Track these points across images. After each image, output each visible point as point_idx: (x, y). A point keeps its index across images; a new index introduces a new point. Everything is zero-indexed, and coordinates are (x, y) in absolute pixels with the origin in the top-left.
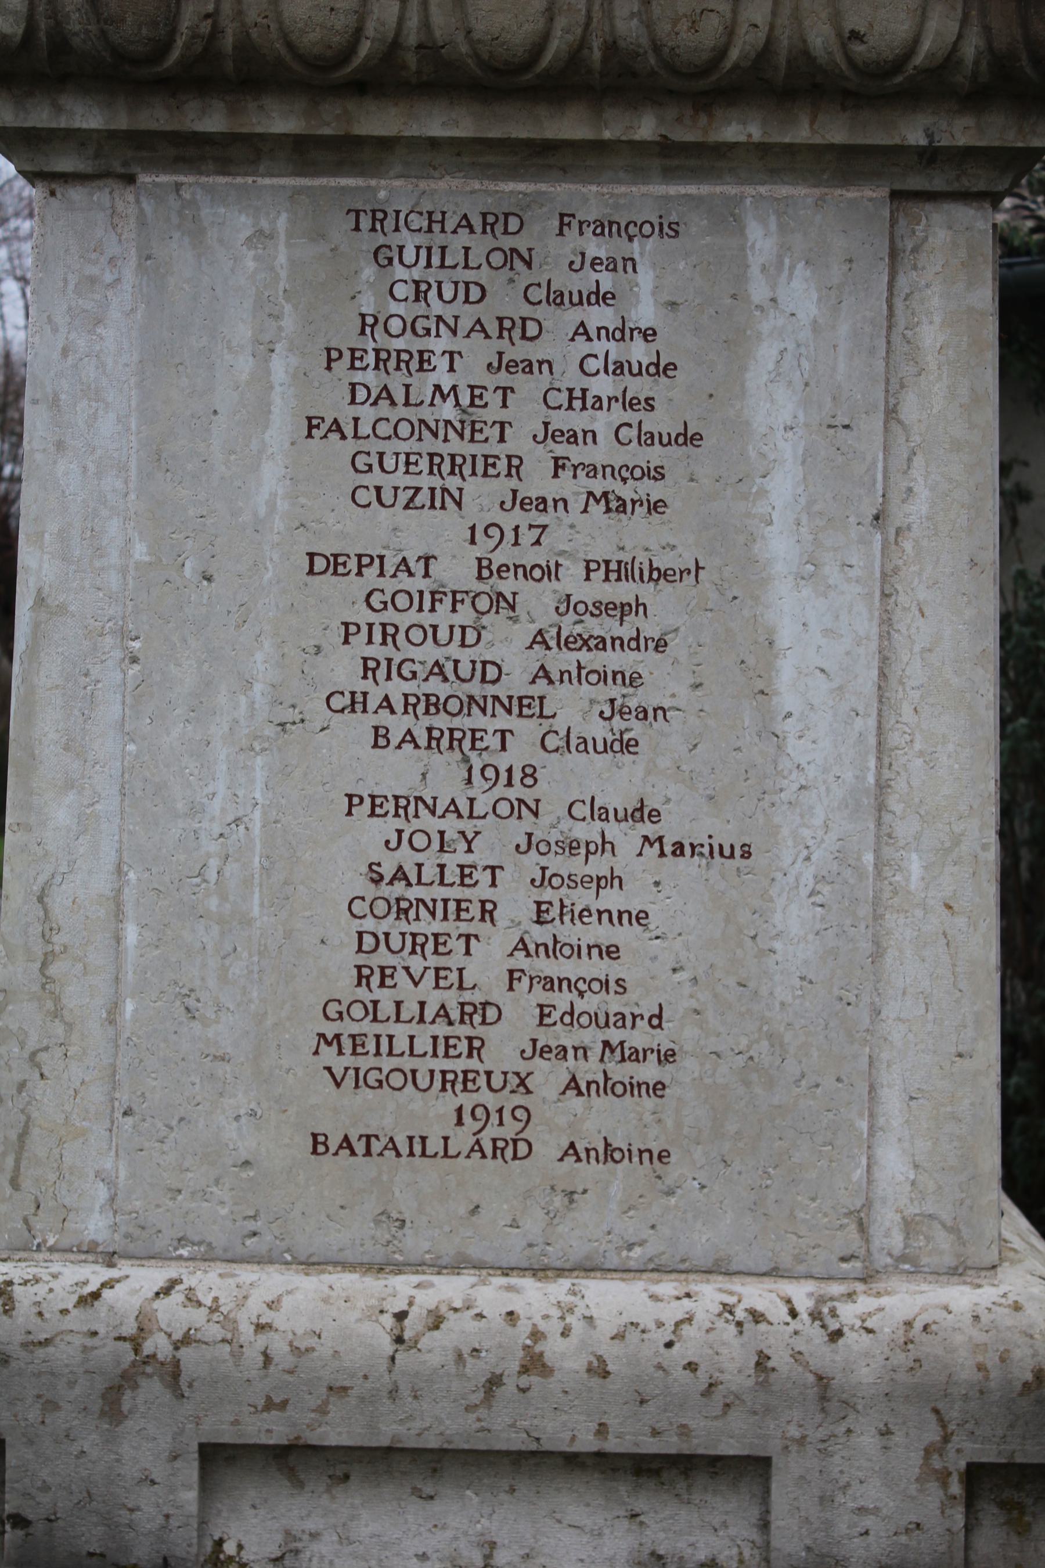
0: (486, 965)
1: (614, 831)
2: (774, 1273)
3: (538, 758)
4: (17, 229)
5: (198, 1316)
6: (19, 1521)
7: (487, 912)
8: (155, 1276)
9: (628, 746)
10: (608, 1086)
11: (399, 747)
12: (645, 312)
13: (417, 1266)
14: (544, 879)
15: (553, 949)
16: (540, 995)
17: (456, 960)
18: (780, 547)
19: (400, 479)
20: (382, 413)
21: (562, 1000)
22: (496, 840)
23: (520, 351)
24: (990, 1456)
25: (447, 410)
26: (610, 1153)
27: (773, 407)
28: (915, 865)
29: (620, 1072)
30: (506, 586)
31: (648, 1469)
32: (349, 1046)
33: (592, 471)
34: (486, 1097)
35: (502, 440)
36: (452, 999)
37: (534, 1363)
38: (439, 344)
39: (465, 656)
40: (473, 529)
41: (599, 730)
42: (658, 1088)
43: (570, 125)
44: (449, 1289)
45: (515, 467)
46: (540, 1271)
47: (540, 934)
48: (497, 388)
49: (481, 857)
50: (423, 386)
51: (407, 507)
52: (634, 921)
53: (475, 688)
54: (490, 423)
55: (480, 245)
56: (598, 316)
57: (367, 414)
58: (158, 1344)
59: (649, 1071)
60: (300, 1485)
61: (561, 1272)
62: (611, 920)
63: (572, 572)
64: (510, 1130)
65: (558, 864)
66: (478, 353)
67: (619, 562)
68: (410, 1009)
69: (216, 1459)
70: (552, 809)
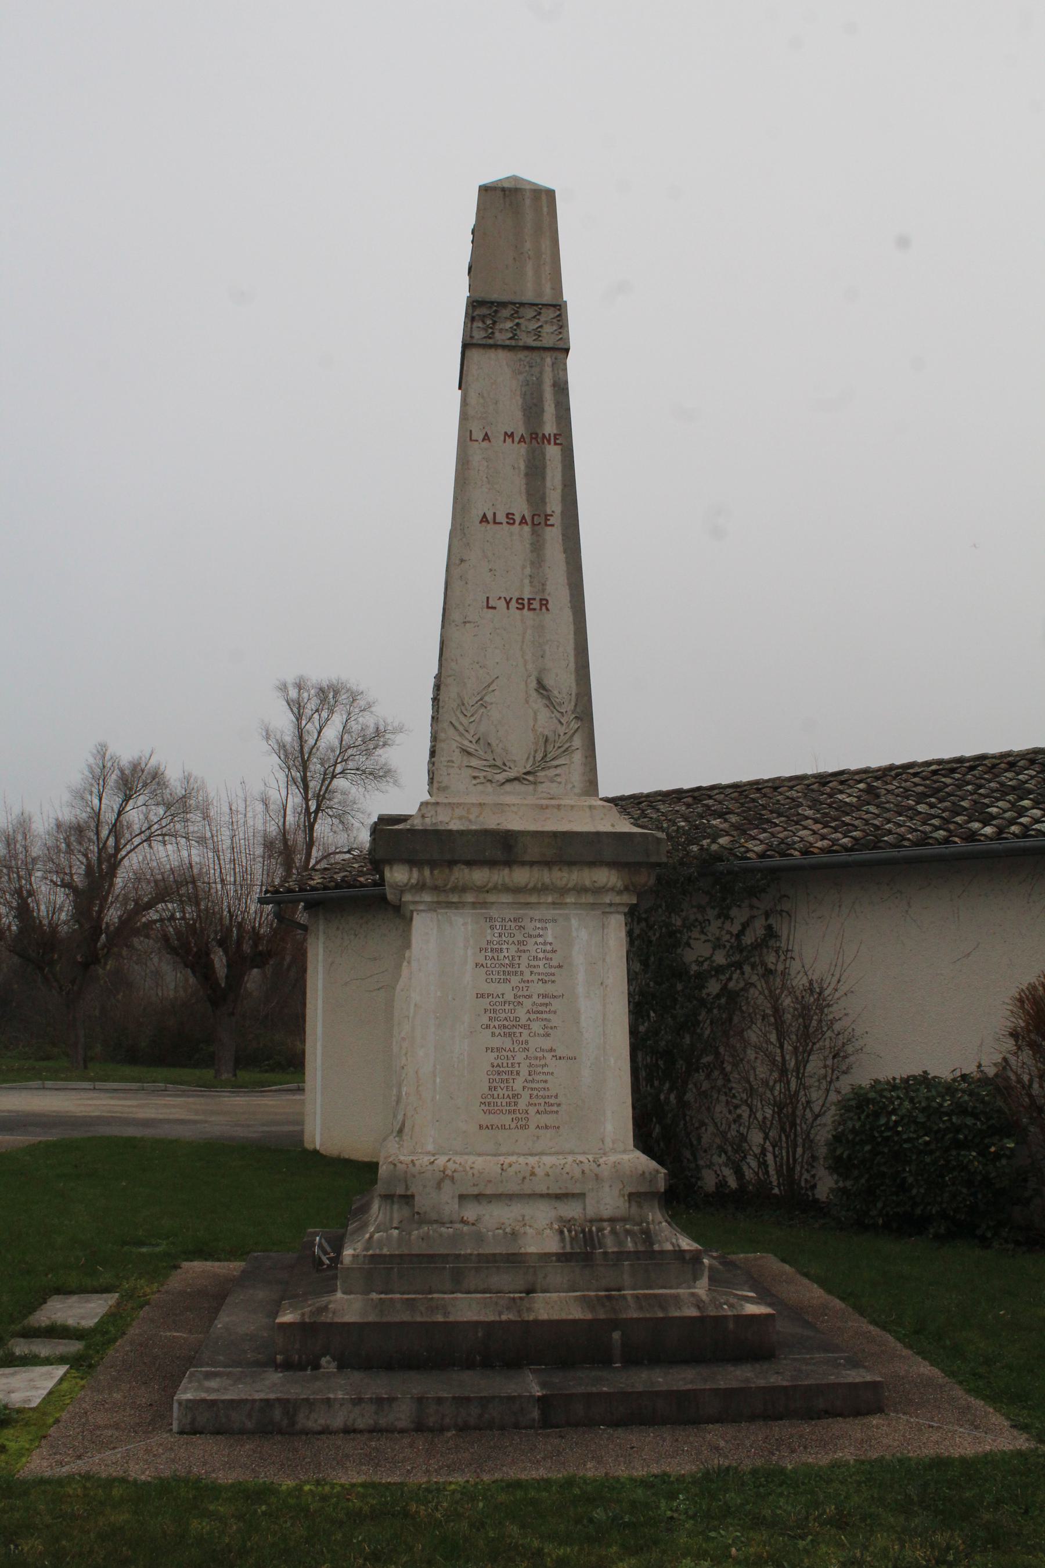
0: (518, 1085)
1: (546, 1054)
2: (584, 1153)
3: (529, 1038)
5: (457, 1166)
6: (418, 1213)
7: (518, 1073)
8: (446, 1158)
9: (548, 1035)
10: (546, 1112)
12: (550, 939)
13: (503, 1155)
14: (531, 1065)
15: (532, 1081)
16: (530, 1092)
17: (511, 1084)
18: (581, 990)
19: (497, 977)
21: (535, 1093)
22: (520, 1057)
23: (523, 948)
24: (634, 1191)
25: (507, 961)
26: (546, 1127)
27: (579, 959)
28: (612, 1060)
29: (548, 1109)
30: (521, 1000)
31: (558, 1197)
32: (488, 1105)
33: (539, 974)
34: (518, 1115)
36: (510, 1093)
37: (533, 1174)
38: (504, 947)
39: (512, 1016)
41: (542, 1032)
42: (557, 1112)
43: (533, 899)
44: (513, 1159)
45: (522, 973)
46: (532, 1155)
47: (530, 1078)
49: (516, 1061)
50: (501, 956)
53: (514, 1023)
55: (513, 925)
56: (539, 940)
57: (489, 962)
58: (449, 1172)
59: (555, 1108)
60: (480, 1203)
61: (536, 1155)
63: (535, 997)
64: (524, 1123)
65: (533, 1062)
66: (513, 948)
68: (501, 1096)
69: (462, 1197)
70: (532, 1050)
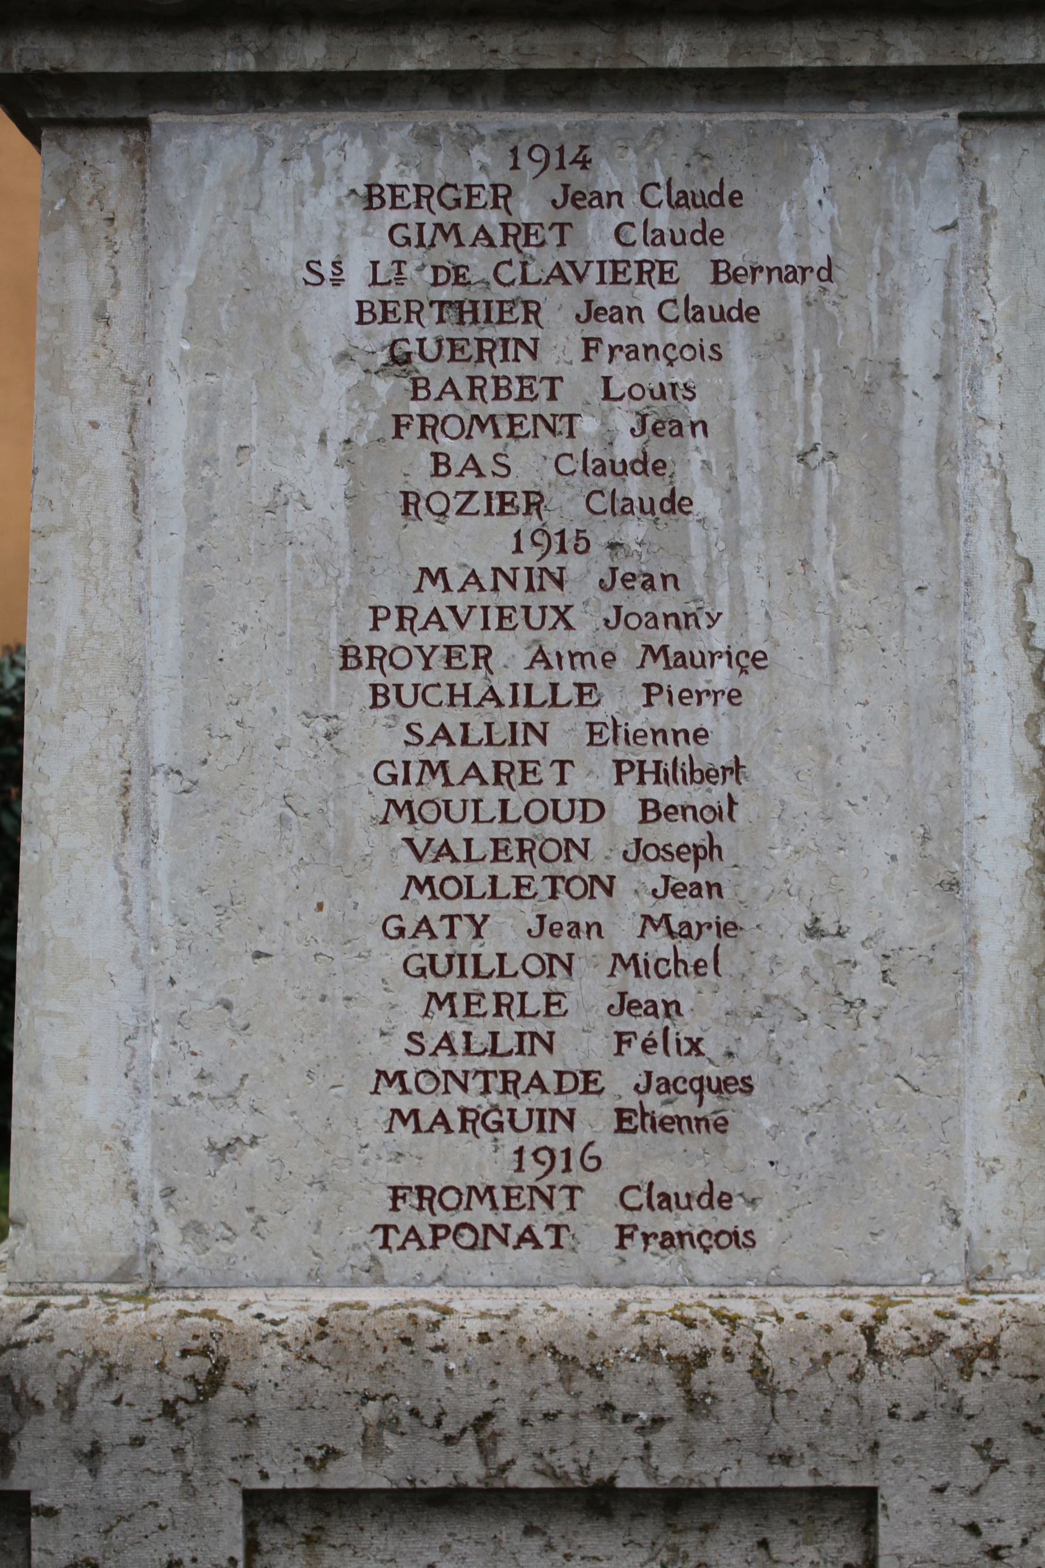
20: (453, 346)
35: (552, 397)
48: (554, 224)
51: (459, 512)
52: (712, 1128)
54: (547, 226)
62: (665, 740)
67: (657, 763)
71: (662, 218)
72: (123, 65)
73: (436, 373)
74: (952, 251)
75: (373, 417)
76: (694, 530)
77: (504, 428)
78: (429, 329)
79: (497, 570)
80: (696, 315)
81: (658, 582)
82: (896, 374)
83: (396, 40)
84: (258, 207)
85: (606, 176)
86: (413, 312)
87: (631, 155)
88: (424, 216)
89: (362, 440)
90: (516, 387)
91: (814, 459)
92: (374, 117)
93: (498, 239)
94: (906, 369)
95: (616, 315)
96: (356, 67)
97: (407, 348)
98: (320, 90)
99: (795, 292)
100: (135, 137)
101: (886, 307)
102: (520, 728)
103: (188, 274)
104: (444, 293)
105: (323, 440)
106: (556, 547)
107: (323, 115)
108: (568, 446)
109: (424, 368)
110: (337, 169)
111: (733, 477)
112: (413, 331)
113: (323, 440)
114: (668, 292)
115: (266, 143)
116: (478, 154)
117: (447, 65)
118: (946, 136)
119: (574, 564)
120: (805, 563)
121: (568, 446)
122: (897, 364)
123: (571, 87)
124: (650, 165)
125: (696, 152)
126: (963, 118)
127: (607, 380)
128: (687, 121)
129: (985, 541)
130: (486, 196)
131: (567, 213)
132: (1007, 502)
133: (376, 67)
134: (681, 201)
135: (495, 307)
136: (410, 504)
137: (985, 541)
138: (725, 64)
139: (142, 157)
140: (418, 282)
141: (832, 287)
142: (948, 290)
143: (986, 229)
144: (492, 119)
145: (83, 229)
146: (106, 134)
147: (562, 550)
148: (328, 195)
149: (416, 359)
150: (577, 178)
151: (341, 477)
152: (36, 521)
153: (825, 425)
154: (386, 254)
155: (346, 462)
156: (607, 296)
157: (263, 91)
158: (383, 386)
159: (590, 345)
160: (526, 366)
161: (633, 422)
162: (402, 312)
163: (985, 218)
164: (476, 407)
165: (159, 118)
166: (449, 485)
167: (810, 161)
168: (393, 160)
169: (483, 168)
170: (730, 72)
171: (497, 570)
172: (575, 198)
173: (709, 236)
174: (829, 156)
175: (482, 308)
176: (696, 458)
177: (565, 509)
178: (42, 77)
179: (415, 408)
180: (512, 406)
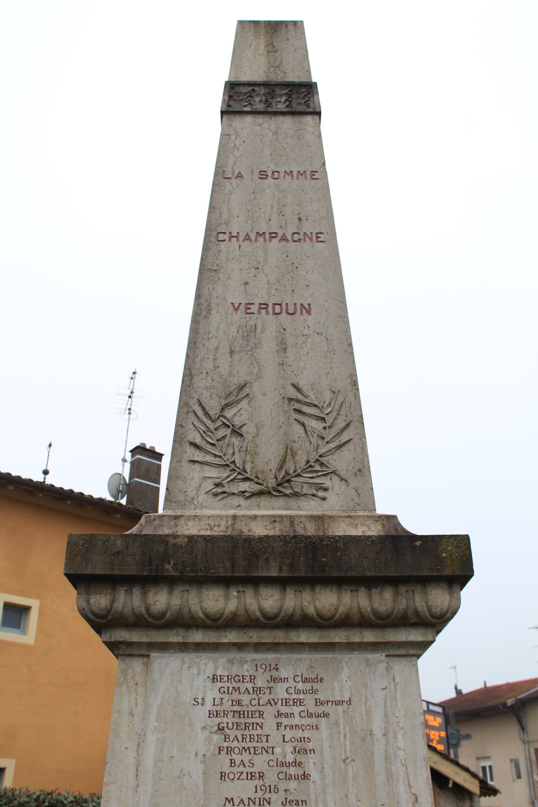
4: (219, 491)
11: (233, 741)
20: (237, 726)
35: (267, 741)
40: (256, 787)
51: (238, 779)
71: (300, 686)
72: (144, 639)
73: (232, 733)
74: (386, 696)
75: (212, 747)
76: (311, 785)
77: (252, 751)
78: (230, 719)
79: (249, 799)
80: (310, 715)
81: (300, 803)
82: (371, 734)
83: (223, 634)
84: (180, 681)
85: (283, 673)
86: (225, 714)
87: (290, 667)
88: (229, 684)
89: (208, 755)
90: (256, 738)
91: (348, 761)
92: (216, 655)
93: (251, 692)
94: (374, 732)
95: (287, 715)
96: (211, 641)
97: (223, 725)
98: (200, 647)
99: (340, 708)
100: (145, 659)
101: (367, 713)
102: (262, 799)
103: (158, 701)
104: (235, 708)
105: (196, 755)
106: (268, 791)
107: (201, 654)
108: (272, 757)
109: (228, 732)
110: (204, 670)
111: (323, 768)
112: (225, 720)
113: (196, 755)
114: (302, 708)
115: (184, 662)
116: (246, 666)
117: (237, 641)
118: (382, 661)
119: (274, 796)
120: (346, 796)
121: (272, 757)
122: (371, 731)
123: (274, 647)
124: (296, 670)
125: (310, 666)
126: (387, 656)
127: (284, 736)
128: (307, 657)
129: (402, 788)
130: (248, 679)
131: (272, 684)
132: (408, 775)
133: (217, 641)
134: (305, 681)
135: (250, 713)
136: (223, 776)
137: (402, 788)
138: (318, 641)
139: (147, 665)
140: (227, 705)
141: (351, 707)
142: (385, 707)
143: (395, 689)
144: (250, 656)
145: (128, 687)
146: (137, 659)
147: (270, 792)
148: (201, 678)
149: (226, 729)
150: (275, 673)
151: (201, 767)
152: (105, 780)
153: (351, 750)
154: (218, 696)
155: (203, 762)
156: (284, 710)
157: (183, 647)
158: (215, 737)
159: (279, 725)
160: (259, 731)
161: (292, 749)
162: (222, 714)
163: (395, 686)
164: (244, 744)
165: (153, 654)
166: (235, 770)
167: (343, 669)
168: (221, 668)
169: (247, 670)
170: (319, 643)
171: (249, 799)
172: (274, 680)
173: (314, 691)
174: (348, 667)
175: (246, 713)
176: (312, 761)
177: (271, 778)
178: (120, 642)
179: (225, 744)
180: (255, 744)
